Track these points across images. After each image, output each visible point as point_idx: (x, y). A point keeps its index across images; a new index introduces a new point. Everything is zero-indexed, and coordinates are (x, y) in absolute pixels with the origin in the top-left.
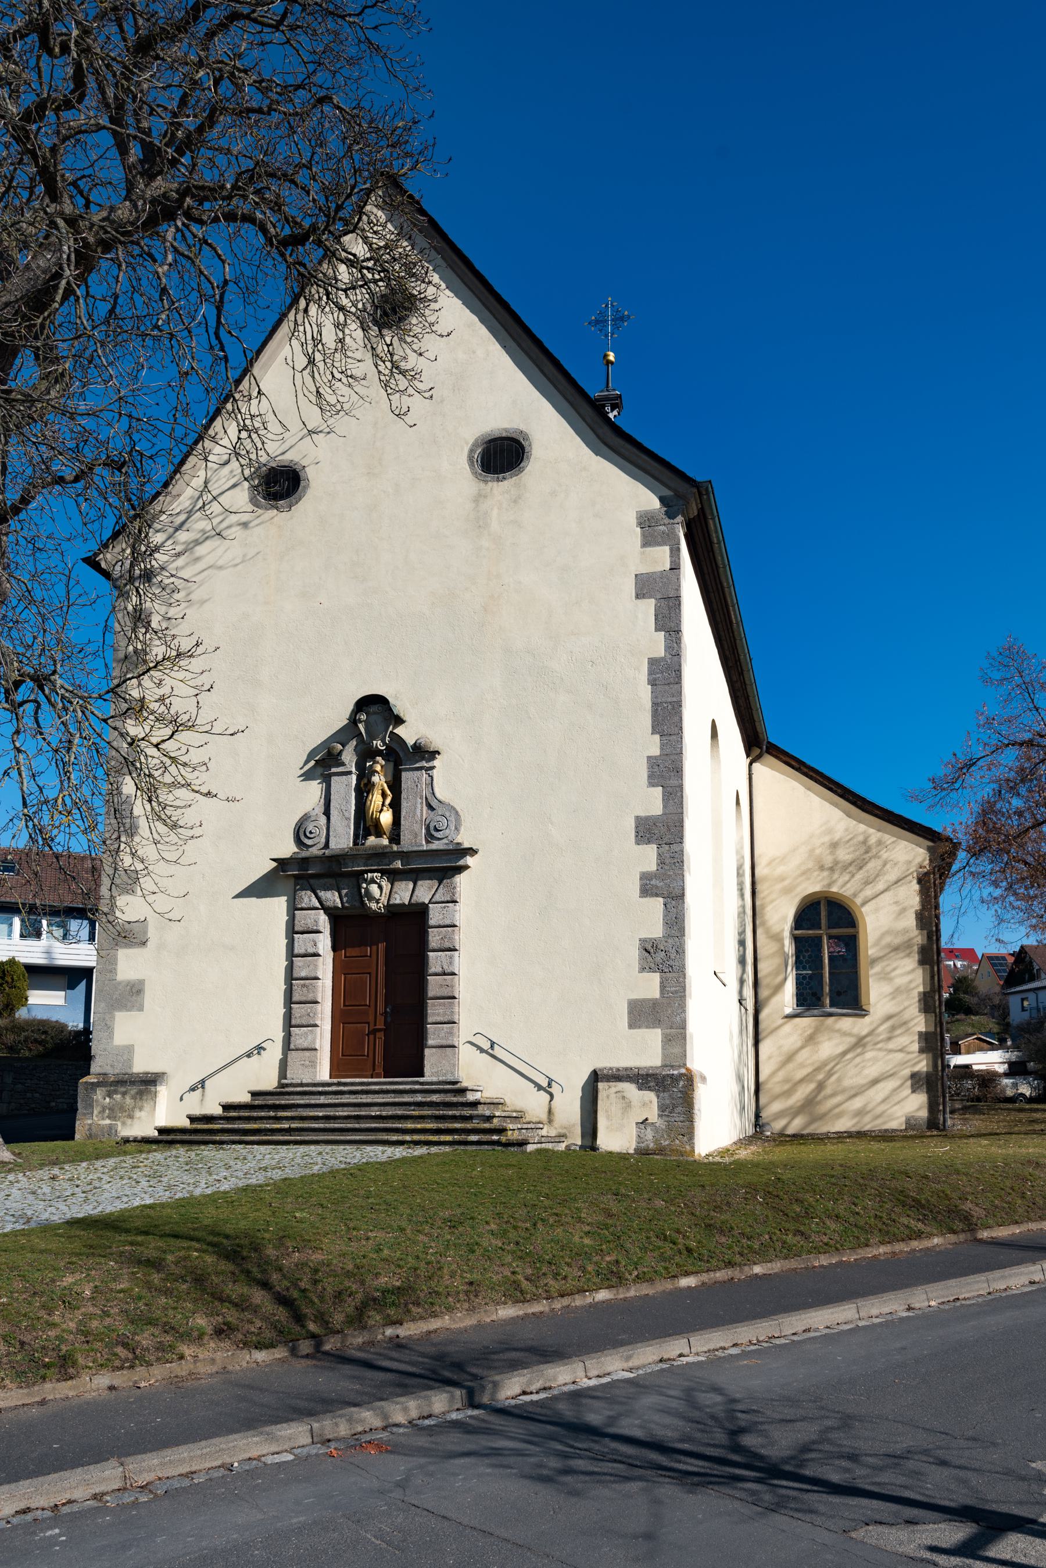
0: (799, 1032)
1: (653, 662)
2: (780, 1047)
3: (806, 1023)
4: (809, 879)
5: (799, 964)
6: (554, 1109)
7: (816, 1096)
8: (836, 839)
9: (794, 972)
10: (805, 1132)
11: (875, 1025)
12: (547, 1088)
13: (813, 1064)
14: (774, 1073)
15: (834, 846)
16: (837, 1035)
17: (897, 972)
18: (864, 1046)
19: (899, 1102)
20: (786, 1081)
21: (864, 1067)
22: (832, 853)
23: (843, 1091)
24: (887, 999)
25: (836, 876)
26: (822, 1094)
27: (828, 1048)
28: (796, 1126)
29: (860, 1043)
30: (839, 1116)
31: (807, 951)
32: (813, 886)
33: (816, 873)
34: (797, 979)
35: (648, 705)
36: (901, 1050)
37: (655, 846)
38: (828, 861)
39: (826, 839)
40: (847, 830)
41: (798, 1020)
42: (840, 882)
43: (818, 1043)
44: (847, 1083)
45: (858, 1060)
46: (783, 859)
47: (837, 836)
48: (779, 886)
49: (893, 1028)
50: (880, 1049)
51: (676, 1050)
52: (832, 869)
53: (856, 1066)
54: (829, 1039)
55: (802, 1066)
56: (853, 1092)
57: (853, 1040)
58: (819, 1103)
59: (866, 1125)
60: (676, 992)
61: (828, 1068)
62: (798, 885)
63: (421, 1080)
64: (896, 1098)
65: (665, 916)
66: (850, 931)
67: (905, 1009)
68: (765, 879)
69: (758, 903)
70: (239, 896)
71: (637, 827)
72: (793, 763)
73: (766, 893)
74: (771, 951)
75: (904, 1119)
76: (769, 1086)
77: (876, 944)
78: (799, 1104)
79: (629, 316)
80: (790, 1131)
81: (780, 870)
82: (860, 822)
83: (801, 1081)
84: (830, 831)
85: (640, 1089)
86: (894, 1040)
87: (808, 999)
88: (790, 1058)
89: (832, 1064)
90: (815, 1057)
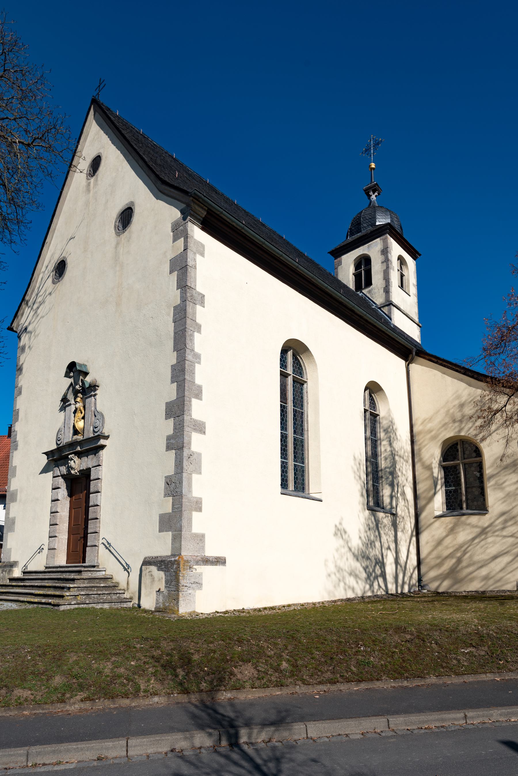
0: (444, 526)
1: (175, 308)
2: (433, 536)
3: (449, 520)
4: (446, 429)
5: (447, 483)
6: (130, 583)
7: (456, 567)
8: (462, 402)
9: (444, 488)
10: (450, 591)
11: (492, 520)
12: (127, 568)
13: (453, 546)
14: (430, 553)
15: (462, 406)
16: (468, 527)
17: (507, 483)
18: (486, 533)
19: (512, 572)
20: (438, 557)
21: (487, 548)
22: (460, 411)
23: (474, 564)
24: (500, 502)
25: (463, 425)
26: (460, 566)
27: (463, 536)
28: (445, 586)
29: (484, 532)
30: (472, 580)
31: (452, 475)
32: (449, 434)
33: (451, 425)
34: (446, 493)
35: (172, 334)
36: (512, 536)
37: (173, 419)
38: (458, 416)
39: (457, 402)
40: (469, 395)
41: (443, 519)
42: (466, 428)
43: (456, 533)
44: (476, 558)
45: (483, 543)
46: (430, 419)
47: (463, 399)
48: (428, 436)
49: (506, 521)
50: (497, 536)
51: (177, 545)
52: (461, 421)
53: (482, 547)
54: (463, 530)
55: (447, 548)
56: (480, 565)
57: (477, 530)
58: (458, 572)
59: (489, 587)
60: (178, 508)
61: (463, 549)
62: (440, 434)
63: (84, 564)
64: (510, 569)
65: (175, 461)
66: (478, 459)
67: (513, 508)
68: (420, 433)
69: (416, 448)
70: (41, 473)
71: (166, 409)
72: (433, 359)
73: (421, 441)
74: (425, 477)
75: (515, 583)
76: (428, 560)
77: (492, 466)
78: (446, 572)
79: (381, 141)
80: (440, 590)
81: (429, 426)
82: (477, 388)
83: (447, 557)
84: (459, 397)
85: (158, 570)
86: (507, 529)
87: (453, 504)
88: (440, 542)
89: (466, 546)
90: (455, 542)
